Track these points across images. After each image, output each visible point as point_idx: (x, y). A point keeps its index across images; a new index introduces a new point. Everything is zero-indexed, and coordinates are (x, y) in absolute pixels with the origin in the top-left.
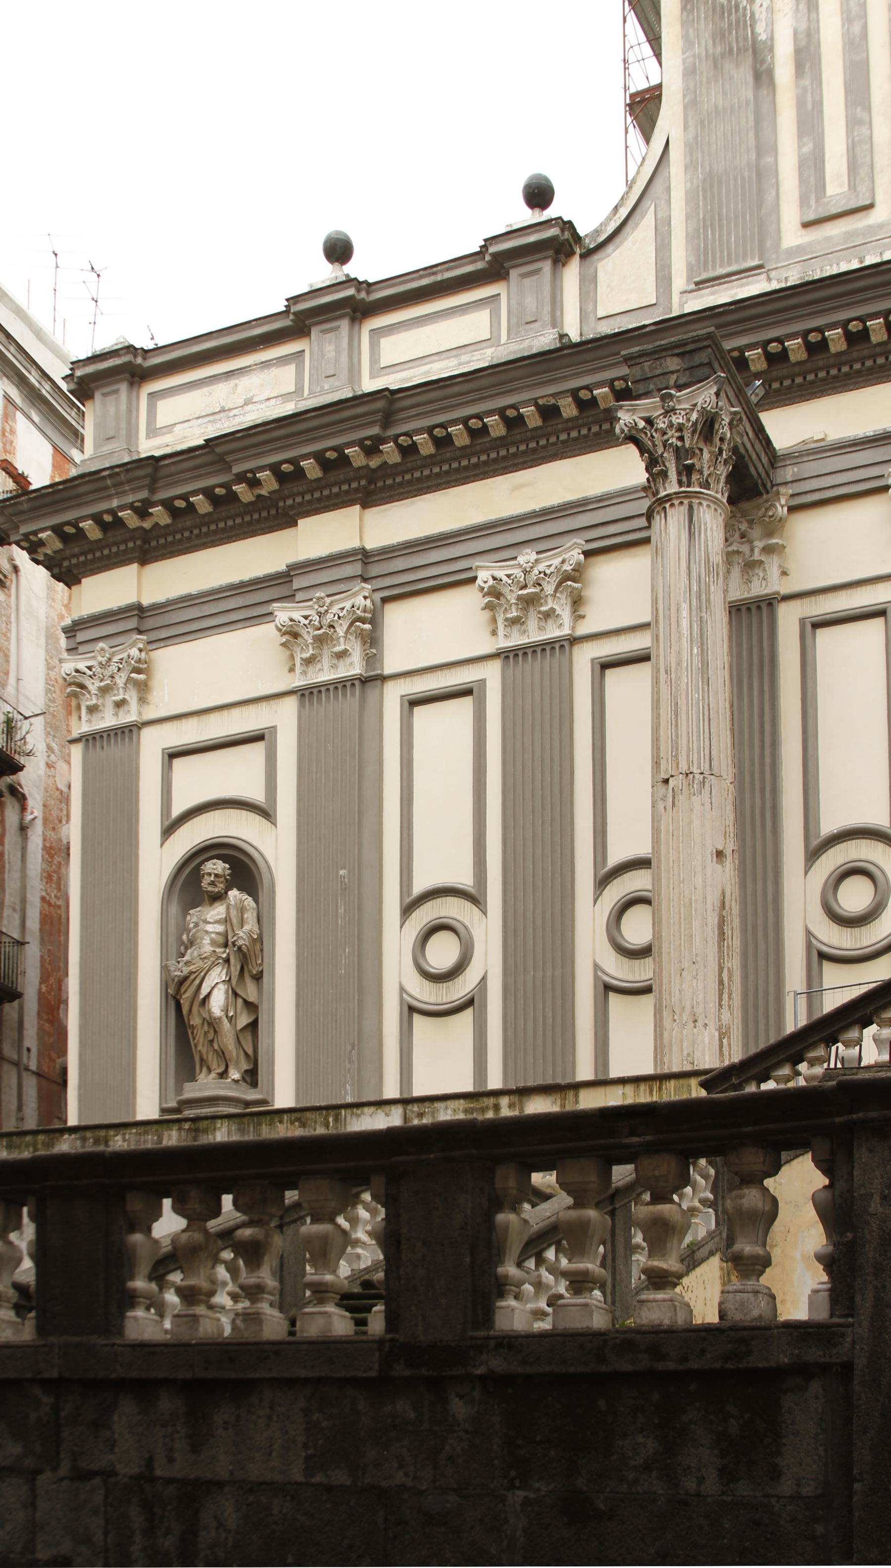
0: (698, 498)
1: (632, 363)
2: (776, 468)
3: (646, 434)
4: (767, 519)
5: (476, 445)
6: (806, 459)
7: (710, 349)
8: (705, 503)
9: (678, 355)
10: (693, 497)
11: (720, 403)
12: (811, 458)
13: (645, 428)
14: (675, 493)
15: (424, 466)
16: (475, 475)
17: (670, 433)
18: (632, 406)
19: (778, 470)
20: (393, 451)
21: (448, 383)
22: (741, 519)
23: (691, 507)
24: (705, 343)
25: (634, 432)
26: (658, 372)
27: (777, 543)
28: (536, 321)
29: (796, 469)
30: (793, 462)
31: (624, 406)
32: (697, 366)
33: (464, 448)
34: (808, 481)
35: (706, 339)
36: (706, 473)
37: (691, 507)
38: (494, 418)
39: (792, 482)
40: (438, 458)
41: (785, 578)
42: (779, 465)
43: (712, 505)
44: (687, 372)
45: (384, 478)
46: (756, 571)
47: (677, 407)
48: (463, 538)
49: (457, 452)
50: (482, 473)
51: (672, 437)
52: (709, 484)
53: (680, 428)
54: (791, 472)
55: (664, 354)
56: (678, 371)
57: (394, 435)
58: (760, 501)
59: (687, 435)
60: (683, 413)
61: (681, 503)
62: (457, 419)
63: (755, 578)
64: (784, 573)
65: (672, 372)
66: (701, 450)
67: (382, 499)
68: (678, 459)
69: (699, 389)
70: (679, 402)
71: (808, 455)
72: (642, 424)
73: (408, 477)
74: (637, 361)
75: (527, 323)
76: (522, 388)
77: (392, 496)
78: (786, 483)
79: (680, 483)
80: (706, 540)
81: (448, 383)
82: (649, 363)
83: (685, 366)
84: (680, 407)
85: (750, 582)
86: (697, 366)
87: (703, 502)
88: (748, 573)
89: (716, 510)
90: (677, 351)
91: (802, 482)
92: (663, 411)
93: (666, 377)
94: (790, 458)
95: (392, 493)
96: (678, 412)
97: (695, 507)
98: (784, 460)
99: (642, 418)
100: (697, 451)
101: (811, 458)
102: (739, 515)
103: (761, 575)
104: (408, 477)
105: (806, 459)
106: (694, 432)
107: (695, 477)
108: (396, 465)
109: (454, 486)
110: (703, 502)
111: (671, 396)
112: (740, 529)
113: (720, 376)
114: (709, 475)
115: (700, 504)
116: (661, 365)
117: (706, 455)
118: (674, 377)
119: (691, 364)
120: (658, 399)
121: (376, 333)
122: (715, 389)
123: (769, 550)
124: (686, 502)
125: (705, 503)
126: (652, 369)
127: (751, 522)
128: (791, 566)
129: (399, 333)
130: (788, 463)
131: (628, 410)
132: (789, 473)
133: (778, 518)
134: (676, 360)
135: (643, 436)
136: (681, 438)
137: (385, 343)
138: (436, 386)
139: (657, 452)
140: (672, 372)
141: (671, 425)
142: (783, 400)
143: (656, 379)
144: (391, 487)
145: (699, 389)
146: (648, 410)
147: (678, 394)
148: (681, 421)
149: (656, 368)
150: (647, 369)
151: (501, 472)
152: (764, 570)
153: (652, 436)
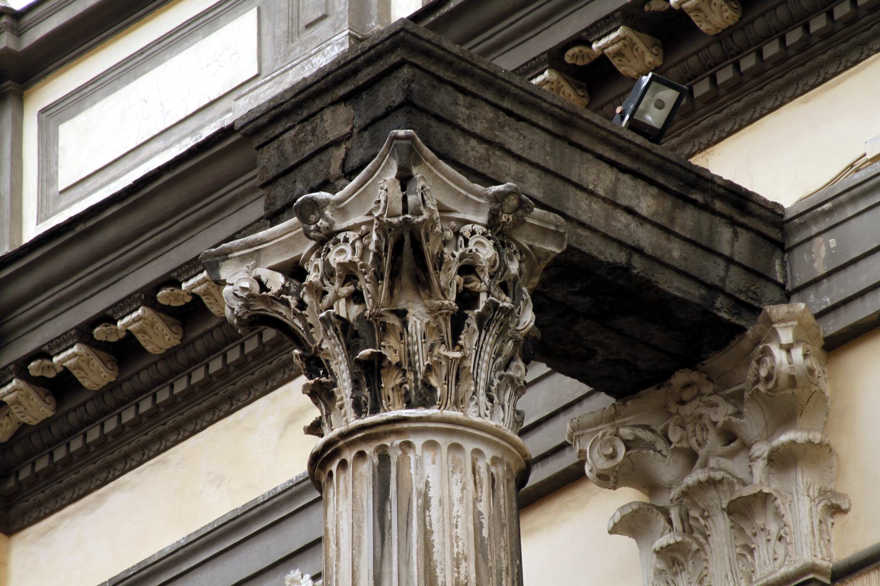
0: (398, 433)
1: (262, 140)
2: (791, 249)
3: (286, 303)
4: (761, 387)
5: (193, 342)
6: (850, 211)
7: (406, 71)
8: (418, 441)
9: (345, 99)
10: (387, 434)
11: (411, 199)
12: (862, 206)
13: (285, 290)
14: (343, 436)
15: (102, 414)
16: (213, 408)
17: (331, 290)
18: (249, 245)
19: (796, 252)
20: (27, 396)
21: (90, 224)
22: (715, 399)
23: (384, 457)
24: (394, 59)
25: (259, 306)
26: (308, 149)
27: (793, 442)
28: (324, 17)
29: (833, 243)
30: (823, 226)
31: (232, 250)
32: (384, 116)
33: (170, 354)
34: (862, 264)
35: (392, 49)
36: (422, 362)
37: (384, 457)
38: (200, 277)
39: (829, 274)
40: (126, 386)
41: (839, 520)
42: (797, 240)
43: (438, 439)
44: (366, 134)
45: (30, 456)
46: (759, 522)
47: (338, 226)
48: (185, 567)
49: (161, 366)
50: (223, 401)
51: (337, 298)
52: (432, 389)
53: (349, 274)
54: (823, 252)
55: (318, 104)
56: (348, 137)
57: (16, 363)
58: (745, 344)
59: (365, 285)
60: (352, 236)
61: (361, 455)
62: (129, 297)
63: (761, 539)
64: (835, 510)
65: (336, 143)
66: (402, 314)
67: (39, 504)
68: (351, 349)
69: (371, 174)
70: (342, 210)
71: (854, 200)
72: (277, 281)
73: (76, 444)
74: (271, 133)
75: (308, 26)
76: (244, 195)
77: (56, 495)
78: (816, 281)
79: (358, 408)
80: (426, 534)
81: (90, 224)
82: (292, 132)
83: (359, 123)
84: (344, 225)
85: (751, 551)
86: (384, 116)
87: (412, 439)
88: (742, 530)
89: (456, 447)
90: (342, 91)
91: (851, 270)
92: (312, 243)
93: (324, 157)
94: (815, 220)
95: (56, 487)
96: (341, 236)
97: (395, 456)
98: (804, 225)
99: (274, 269)
100: (393, 320)
101: (862, 206)
102: (708, 389)
103: (773, 528)
104: (76, 444)
105: (850, 211)
106: (378, 276)
107: (390, 382)
108: (46, 424)
109: (176, 443)
110: (412, 439)
111: (316, 206)
112: (715, 424)
113: (396, 138)
114: (429, 368)
115: (409, 445)
116: (314, 131)
117: (418, 318)
118: (340, 153)
119: (371, 115)
120: (295, 220)
121: (53, 115)
122: (392, 174)
123: (783, 461)
124: (369, 449)
125: (418, 441)
126: (298, 144)
127: (738, 398)
128: (853, 487)
129: (94, 103)
130: (815, 230)
131: (243, 259)
132: (820, 255)
133: (783, 379)
134: (344, 112)
135: (282, 309)
136: (356, 297)
137: (68, 132)
138: (69, 235)
139: (314, 342)
140: (336, 143)
141: (329, 273)
142: (800, 78)
143: (307, 167)
144: (50, 473)
145: (371, 174)
146: (287, 245)
147: (339, 195)
148: (348, 257)
149: (305, 142)
150: (288, 148)
151: (261, 387)
152: (779, 516)
153: (302, 305)
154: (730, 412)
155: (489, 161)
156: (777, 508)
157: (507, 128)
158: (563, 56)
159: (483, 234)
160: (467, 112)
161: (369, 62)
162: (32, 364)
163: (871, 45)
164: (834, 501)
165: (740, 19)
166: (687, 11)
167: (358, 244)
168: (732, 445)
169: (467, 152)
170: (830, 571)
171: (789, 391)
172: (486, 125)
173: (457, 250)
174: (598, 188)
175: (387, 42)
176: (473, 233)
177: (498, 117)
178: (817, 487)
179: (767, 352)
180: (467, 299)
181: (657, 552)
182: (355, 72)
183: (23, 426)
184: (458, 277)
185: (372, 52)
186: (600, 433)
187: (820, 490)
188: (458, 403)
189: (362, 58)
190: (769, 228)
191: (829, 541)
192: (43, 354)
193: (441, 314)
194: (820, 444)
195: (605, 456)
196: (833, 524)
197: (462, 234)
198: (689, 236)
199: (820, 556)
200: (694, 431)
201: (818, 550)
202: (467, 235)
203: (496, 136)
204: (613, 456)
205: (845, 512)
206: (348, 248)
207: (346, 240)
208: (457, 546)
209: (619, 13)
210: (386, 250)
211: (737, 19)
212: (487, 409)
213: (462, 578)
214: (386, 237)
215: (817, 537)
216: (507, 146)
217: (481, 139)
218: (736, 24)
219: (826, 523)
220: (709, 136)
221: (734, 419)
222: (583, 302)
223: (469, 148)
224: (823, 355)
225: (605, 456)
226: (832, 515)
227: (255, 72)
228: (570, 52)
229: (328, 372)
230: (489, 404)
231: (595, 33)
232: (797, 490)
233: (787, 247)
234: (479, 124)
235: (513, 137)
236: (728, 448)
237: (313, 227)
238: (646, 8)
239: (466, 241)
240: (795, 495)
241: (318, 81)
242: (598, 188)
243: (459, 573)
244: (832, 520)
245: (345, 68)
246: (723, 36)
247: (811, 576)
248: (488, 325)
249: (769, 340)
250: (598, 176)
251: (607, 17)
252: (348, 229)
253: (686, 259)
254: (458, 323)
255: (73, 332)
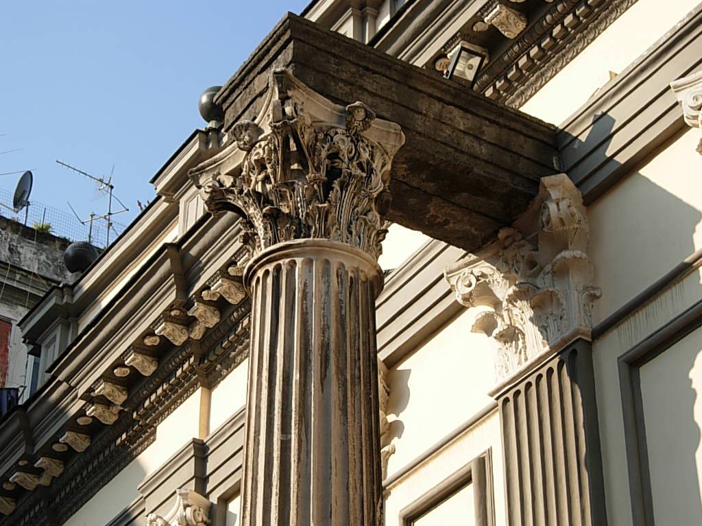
0: (287, 256)
10: (280, 257)
41: (596, 303)
51: (257, 182)
55: (252, 75)
96: (257, 145)
126: (242, 102)
154: (531, 249)
155: (352, 95)
156: (558, 300)
157: (365, 77)
158: (435, 67)
159: (343, 134)
160: (337, 67)
161: (274, 44)
162: (203, 293)
163: (599, 28)
164: (592, 292)
165: (527, 26)
166: (496, 25)
167: (266, 148)
168: (535, 269)
169: (336, 90)
170: (590, 333)
171: (561, 228)
172: (349, 75)
173: (326, 144)
174: (429, 113)
175: (282, 28)
176: (336, 133)
177: (359, 71)
178: (582, 285)
179: (546, 207)
180: (333, 173)
181: (495, 338)
182: (268, 51)
183: (208, 329)
184: (326, 160)
185: (275, 36)
186: (462, 274)
187: (584, 287)
188: (327, 234)
189: (270, 41)
190: (551, 143)
191: (590, 316)
192: (206, 287)
193: (316, 183)
194: (581, 258)
195: (465, 286)
196: (592, 306)
197: (329, 135)
198: (493, 141)
199: (584, 325)
200: (513, 265)
201: (583, 321)
202: (332, 134)
203: (357, 81)
204: (470, 285)
205: (598, 297)
206: (261, 151)
207: (260, 146)
208: (324, 321)
209: (459, 34)
210: (279, 146)
211: (524, 27)
212: (348, 238)
213: (326, 339)
214: (277, 137)
215: (583, 314)
216: (365, 87)
217: (346, 82)
218: (525, 29)
219: (588, 305)
220: (520, 100)
221: (533, 252)
222: (431, 187)
223: (337, 88)
224: (585, 208)
225: (465, 286)
226: (592, 301)
227: (648, 373)
228: (438, 63)
229: (252, 226)
230: (349, 236)
231: (448, 48)
232: (569, 288)
233: (559, 149)
234: (345, 74)
235: (369, 82)
236: (532, 271)
237: (242, 142)
238: (475, 29)
239: (332, 138)
240: (568, 291)
241: (250, 62)
242: (429, 113)
243: (324, 337)
244: (592, 304)
245: (263, 50)
246: (519, 38)
247: (578, 337)
248: (347, 187)
249: (547, 199)
250: (430, 107)
251: (453, 37)
252: (262, 140)
253: (491, 155)
254: (328, 187)
255: (218, 272)
